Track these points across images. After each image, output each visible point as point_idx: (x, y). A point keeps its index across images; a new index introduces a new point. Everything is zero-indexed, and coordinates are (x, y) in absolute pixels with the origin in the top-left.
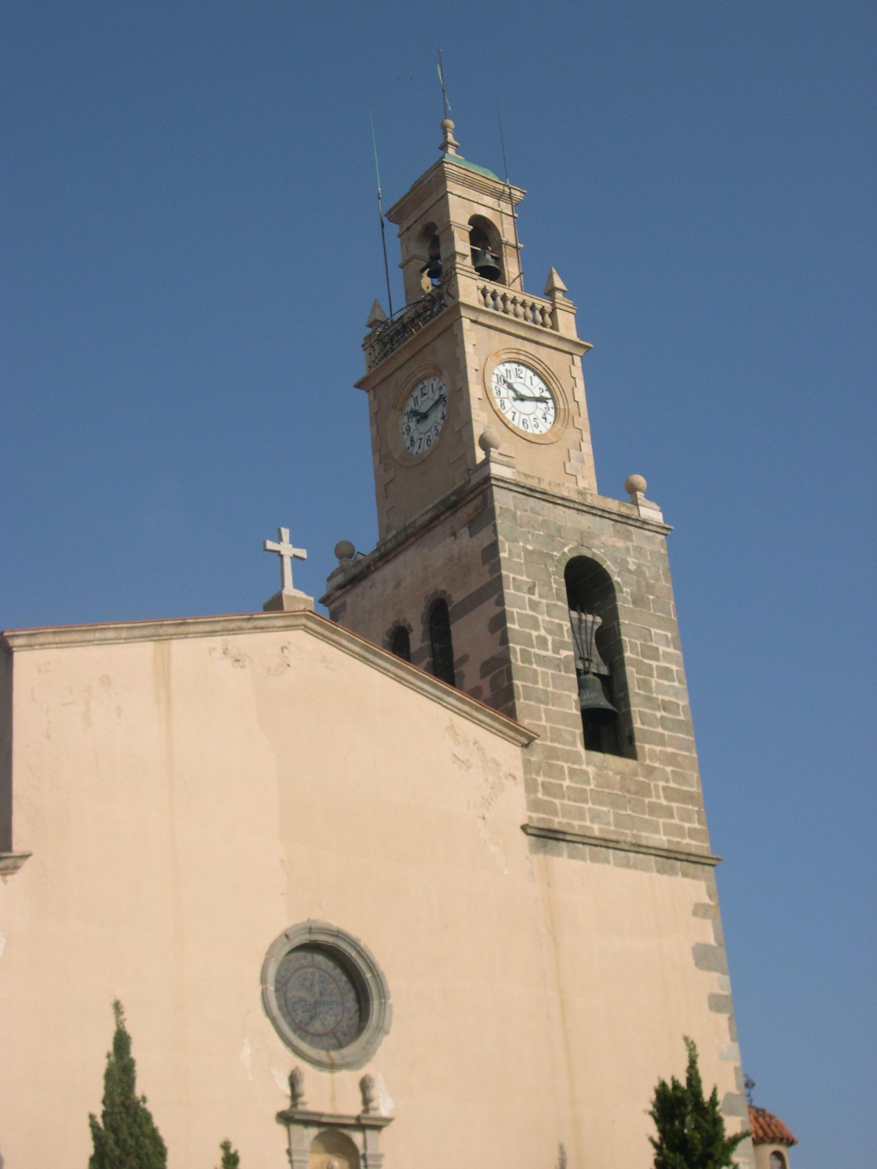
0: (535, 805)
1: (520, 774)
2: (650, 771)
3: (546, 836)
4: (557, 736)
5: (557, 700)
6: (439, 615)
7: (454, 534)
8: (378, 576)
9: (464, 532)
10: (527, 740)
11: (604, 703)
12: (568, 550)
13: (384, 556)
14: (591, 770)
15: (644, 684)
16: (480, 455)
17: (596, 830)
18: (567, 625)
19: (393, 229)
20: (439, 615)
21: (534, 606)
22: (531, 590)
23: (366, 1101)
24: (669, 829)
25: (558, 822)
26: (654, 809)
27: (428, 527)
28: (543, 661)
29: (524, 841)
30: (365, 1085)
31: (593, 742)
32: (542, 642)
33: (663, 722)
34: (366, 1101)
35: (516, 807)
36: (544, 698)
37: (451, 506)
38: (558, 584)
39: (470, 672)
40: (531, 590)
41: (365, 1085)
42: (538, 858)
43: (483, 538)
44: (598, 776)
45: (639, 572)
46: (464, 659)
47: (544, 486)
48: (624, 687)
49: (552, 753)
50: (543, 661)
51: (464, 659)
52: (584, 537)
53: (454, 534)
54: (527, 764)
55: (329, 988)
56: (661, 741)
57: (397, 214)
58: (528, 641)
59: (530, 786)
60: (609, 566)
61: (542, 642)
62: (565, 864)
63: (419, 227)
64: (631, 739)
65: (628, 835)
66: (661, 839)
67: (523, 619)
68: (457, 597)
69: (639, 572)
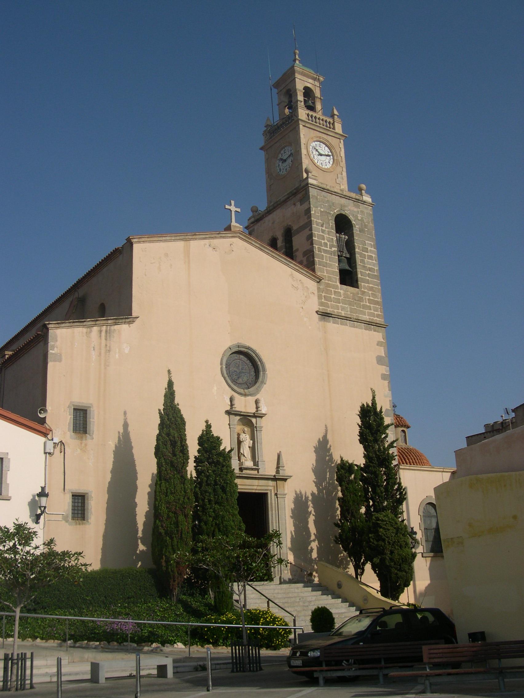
0: (321, 304)
1: (316, 292)
2: (363, 293)
3: (325, 315)
4: (330, 279)
5: (330, 266)
6: (288, 234)
7: (295, 204)
8: (266, 219)
9: (298, 204)
10: (319, 280)
11: (347, 267)
12: (336, 211)
13: (269, 212)
14: (342, 292)
15: (362, 261)
16: (305, 175)
17: (343, 313)
18: (335, 239)
19: (275, 91)
20: (288, 234)
21: (323, 231)
22: (322, 226)
23: (257, 408)
24: (370, 314)
25: (329, 310)
26: (365, 307)
27: (285, 201)
28: (326, 251)
29: (317, 316)
30: (257, 402)
31: (343, 281)
32: (326, 245)
33: (369, 275)
34: (257, 408)
35: (314, 304)
36: (326, 265)
37: (294, 194)
38: (332, 223)
39: (299, 255)
40: (322, 226)
41: (257, 402)
42: (322, 323)
43: (305, 206)
44: (344, 294)
45: (362, 220)
46: (297, 250)
47: (328, 187)
48: (355, 262)
49: (328, 285)
50: (326, 251)
51: (297, 250)
52: (342, 207)
53: (295, 204)
54: (319, 289)
55: (245, 367)
56: (368, 282)
57: (277, 85)
58: (320, 244)
59: (320, 297)
60: (351, 217)
61: (326, 245)
62: (331, 326)
63: (285, 90)
64: (357, 281)
65: (354, 316)
66: (366, 318)
67: (319, 236)
68: (295, 228)
69: (362, 220)
